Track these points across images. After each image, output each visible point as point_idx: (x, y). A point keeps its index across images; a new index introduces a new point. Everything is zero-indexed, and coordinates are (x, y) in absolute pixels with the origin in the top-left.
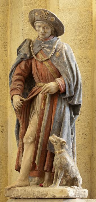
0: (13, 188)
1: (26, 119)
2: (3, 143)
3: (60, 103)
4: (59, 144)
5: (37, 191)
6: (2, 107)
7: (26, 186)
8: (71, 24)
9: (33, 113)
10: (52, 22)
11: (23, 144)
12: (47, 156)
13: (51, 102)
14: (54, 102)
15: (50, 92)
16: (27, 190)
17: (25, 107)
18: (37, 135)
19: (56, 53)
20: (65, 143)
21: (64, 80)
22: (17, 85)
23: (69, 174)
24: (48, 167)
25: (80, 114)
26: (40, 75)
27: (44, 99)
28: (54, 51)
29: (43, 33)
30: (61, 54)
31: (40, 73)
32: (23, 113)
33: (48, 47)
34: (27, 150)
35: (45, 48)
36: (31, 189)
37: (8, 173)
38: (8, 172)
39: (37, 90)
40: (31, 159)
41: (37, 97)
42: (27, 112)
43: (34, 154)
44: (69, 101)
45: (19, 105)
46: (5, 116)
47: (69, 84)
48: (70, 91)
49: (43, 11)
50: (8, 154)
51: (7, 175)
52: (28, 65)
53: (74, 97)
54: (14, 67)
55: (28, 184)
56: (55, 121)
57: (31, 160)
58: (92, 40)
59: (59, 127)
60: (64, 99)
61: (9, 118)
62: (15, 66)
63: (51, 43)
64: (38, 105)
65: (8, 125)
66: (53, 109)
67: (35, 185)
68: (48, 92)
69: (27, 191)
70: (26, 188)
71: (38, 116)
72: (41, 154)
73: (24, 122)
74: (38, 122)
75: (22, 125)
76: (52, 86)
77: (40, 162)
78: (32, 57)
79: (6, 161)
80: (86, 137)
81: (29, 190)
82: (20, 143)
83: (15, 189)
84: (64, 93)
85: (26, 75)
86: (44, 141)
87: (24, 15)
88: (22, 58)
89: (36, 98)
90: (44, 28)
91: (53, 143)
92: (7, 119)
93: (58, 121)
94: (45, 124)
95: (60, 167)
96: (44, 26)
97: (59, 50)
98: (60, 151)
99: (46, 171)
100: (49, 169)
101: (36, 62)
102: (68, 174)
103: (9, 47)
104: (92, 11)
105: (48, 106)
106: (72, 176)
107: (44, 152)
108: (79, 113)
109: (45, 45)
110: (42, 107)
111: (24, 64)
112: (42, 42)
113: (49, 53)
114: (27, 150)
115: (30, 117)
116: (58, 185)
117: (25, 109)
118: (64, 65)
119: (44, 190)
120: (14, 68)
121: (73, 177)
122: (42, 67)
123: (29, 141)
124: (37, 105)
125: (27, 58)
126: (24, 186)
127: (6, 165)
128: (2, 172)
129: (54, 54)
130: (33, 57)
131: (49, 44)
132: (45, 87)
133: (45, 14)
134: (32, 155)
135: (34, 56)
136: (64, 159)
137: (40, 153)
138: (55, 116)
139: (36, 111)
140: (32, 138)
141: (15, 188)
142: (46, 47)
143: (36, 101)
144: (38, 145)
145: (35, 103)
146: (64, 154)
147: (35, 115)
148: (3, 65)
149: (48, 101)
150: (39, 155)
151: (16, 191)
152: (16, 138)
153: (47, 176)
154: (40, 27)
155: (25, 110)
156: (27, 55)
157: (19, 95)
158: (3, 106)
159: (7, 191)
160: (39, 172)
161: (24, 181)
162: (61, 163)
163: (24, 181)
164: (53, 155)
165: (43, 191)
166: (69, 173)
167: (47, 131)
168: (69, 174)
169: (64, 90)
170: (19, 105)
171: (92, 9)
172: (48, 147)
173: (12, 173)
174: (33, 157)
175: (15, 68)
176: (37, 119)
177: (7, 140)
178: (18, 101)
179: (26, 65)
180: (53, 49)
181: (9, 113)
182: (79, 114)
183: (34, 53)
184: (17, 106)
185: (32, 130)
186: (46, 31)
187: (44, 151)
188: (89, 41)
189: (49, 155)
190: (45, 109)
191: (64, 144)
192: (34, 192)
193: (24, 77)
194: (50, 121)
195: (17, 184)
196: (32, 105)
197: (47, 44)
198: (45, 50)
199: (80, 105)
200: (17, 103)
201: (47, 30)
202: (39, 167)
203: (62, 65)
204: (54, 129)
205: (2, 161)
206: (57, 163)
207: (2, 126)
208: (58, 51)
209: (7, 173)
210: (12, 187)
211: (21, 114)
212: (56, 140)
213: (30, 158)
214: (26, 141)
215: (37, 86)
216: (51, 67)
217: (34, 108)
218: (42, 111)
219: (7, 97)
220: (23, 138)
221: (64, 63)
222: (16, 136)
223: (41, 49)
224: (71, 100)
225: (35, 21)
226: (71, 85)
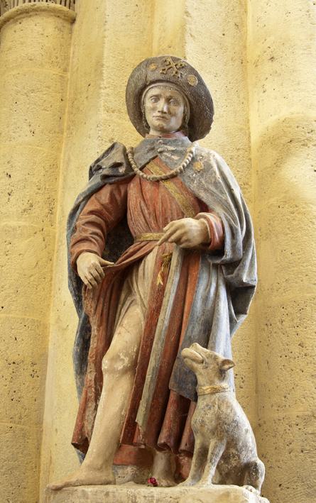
0: (71, 488)
1: (109, 314)
2: (34, 399)
3: (205, 276)
4: (214, 367)
5: (145, 497)
6: (36, 324)
7: (108, 483)
8: (209, 145)
9: (128, 303)
10: (190, 85)
11: (99, 379)
12: (168, 408)
13: (183, 265)
14: (190, 272)
15: (184, 238)
16: (114, 492)
17: (107, 289)
18: (142, 351)
19: (194, 164)
20: (231, 366)
21: (220, 218)
22: (90, 232)
23: (237, 450)
24: (169, 436)
25: (248, 312)
26: (149, 214)
27: (165, 263)
28: (190, 159)
29: (165, 113)
30: (208, 167)
31: (151, 209)
32: (102, 300)
33: (173, 151)
34: (111, 390)
35: (165, 154)
36: (125, 490)
37: (42, 467)
38: (42, 465)
39: (142, 247)
40: (123, 413)
41: (142, 264)
42: (113, 297)
43: (133, 400)
44: (229, 274)
45: (96, 274)
46: (42, 343)
47: (231, 227)
48: (234, 246)
49: (169, 60)
50: (44, 424)
51: (39, 472)
52: (118, 197)
53: (241, 264)
54: (82, 198)
55: (111, 478)
56: (192, 316)
57: (122, 416)
58: (251, 186)
59: (205, 331)
60: (216, 266)
61: (50, 346)
62: (84, 196)
63: (180, 143)
64: (143, 285)
65: (47, 363)
66: (188, 289)
67: (132, 483)
68: (178, 241)
69: (114, 496)
70: (110, 488)
71: (144, 308)
72: (153, 401)
73: (104, 324)
74: (143, 323)
75: (98, 331)
76: (192, 226)
77: (148, 420)
78: (131, 173)
79: (38, 441)
80: (242, 384)
81: (119, 493)
82: (90, 376)
83: (76, 490)
84: (220, 251)
85: (112, 218)
86: (161, 367)
87: (102, 128)
88: (105, 177)
89: (138, 270)
90: (168, 100)
91: (195, 365)
92: (46, 348)
93: (202, 319)
94: (166, 323)
95: (216, 428)
96: (168, 94)
98: (215, 387)
99: (163, 447)
100: (171, 443)
102: (234, 451)
103: (59, 206)
104: (250, 133)
105: (174, 277)
106: (244, 460)
107: (162, 394)
108: (246, 310)
109: (166, 146)
110: (159, 281)
111: (109, 192)
112: (158, 140)
113: (176, 164)
114: (111, 390)
115: (117, 316)
116: (210, 480)
117: (106, 291)
118: (217, 188)
119: (167, 494)
120: (83, 200)
121: (245, 461)
122: (158, 193)
123: (120, 366)
124: (139, 280)
125: (115, 176)
126: (101, 484)
127: (38, 448)
128: (27, 463)
129: (188, 166)
130: (135, 175)
131: (177, 146)
132: (172, 226)
133: (176, 65)
134: (126, 402)
135: (137, 170)
136: (228, 407)
137: (149, 396)
138: (192, 304)
139: (138, 296)
140: (127, 360)
141: (75, 488)
142: (168, 151)
143: (137, 275)
144: (144, 378)
145: (134, 278)
146: (227, 394)
147: (136, 306)
148: (44, 240)
149: (177, 266)
150: (147, 401)
151: (79, 494)
152: (76, 371)
153: (160, 461)
154: (157, 98)
155: (108, 295)
156: (117, 170)
157: (96, 253)
158: (37, 321)
159: (52, 496)
160: (140, 450)
161: (100, 469)
162: (218, 418)
163: (100, 469)
164: (185, 406)
165: (163, 495)
166: (239, 448)
167: (169, 343)
168: (237, 450)
169: (220, 241)
170: (96, 274)
171: (249, 128)
172: (172, 383)
173: (52, 465)
174: (129, 408)
175: (84, 202)
176: (141, 316)
177: (43, 394)
178: (92, 262)
179: (114, 195)
180: (189, 154)
181: (51, 331)
182: (246, 314)
183: (136, 164)
184: (90, 277)
185: (127, 340)
186: (171, 111)
187: (160, 395)
188: (246, 186)
189: (175, 405)
190: (168, 286)
191: (230, 368)
192: (135, 498)
193: (106, 222)
194: (178, 316)
195: (82, 479)
196: (125, 286)
197: (170, 145)
198: (167, 157)
199: (253, 287)
200: (89, 268)
201: (175, 107)
202: (145, 435)
203: (212, 188)
204: (190, 337)
205: (28, 439)
206: (206, 420)
207: (33, 364)
208: (200, 160)
209: (39, 467)
210: (67, 485)
211: (98, 300)
212: (204, 356)
213: (121, 409)
214: (111, 366)
215: (142, 242)
216: (182, 194)
217: (130, 292)
218: (159, 293)
219: (49, 305)
220: (101, 360)
221: (216, 184)
222: (76, 365)
223: (157, 156)
224: (232, 273)
225: (145, 86)
226: (237, 230)
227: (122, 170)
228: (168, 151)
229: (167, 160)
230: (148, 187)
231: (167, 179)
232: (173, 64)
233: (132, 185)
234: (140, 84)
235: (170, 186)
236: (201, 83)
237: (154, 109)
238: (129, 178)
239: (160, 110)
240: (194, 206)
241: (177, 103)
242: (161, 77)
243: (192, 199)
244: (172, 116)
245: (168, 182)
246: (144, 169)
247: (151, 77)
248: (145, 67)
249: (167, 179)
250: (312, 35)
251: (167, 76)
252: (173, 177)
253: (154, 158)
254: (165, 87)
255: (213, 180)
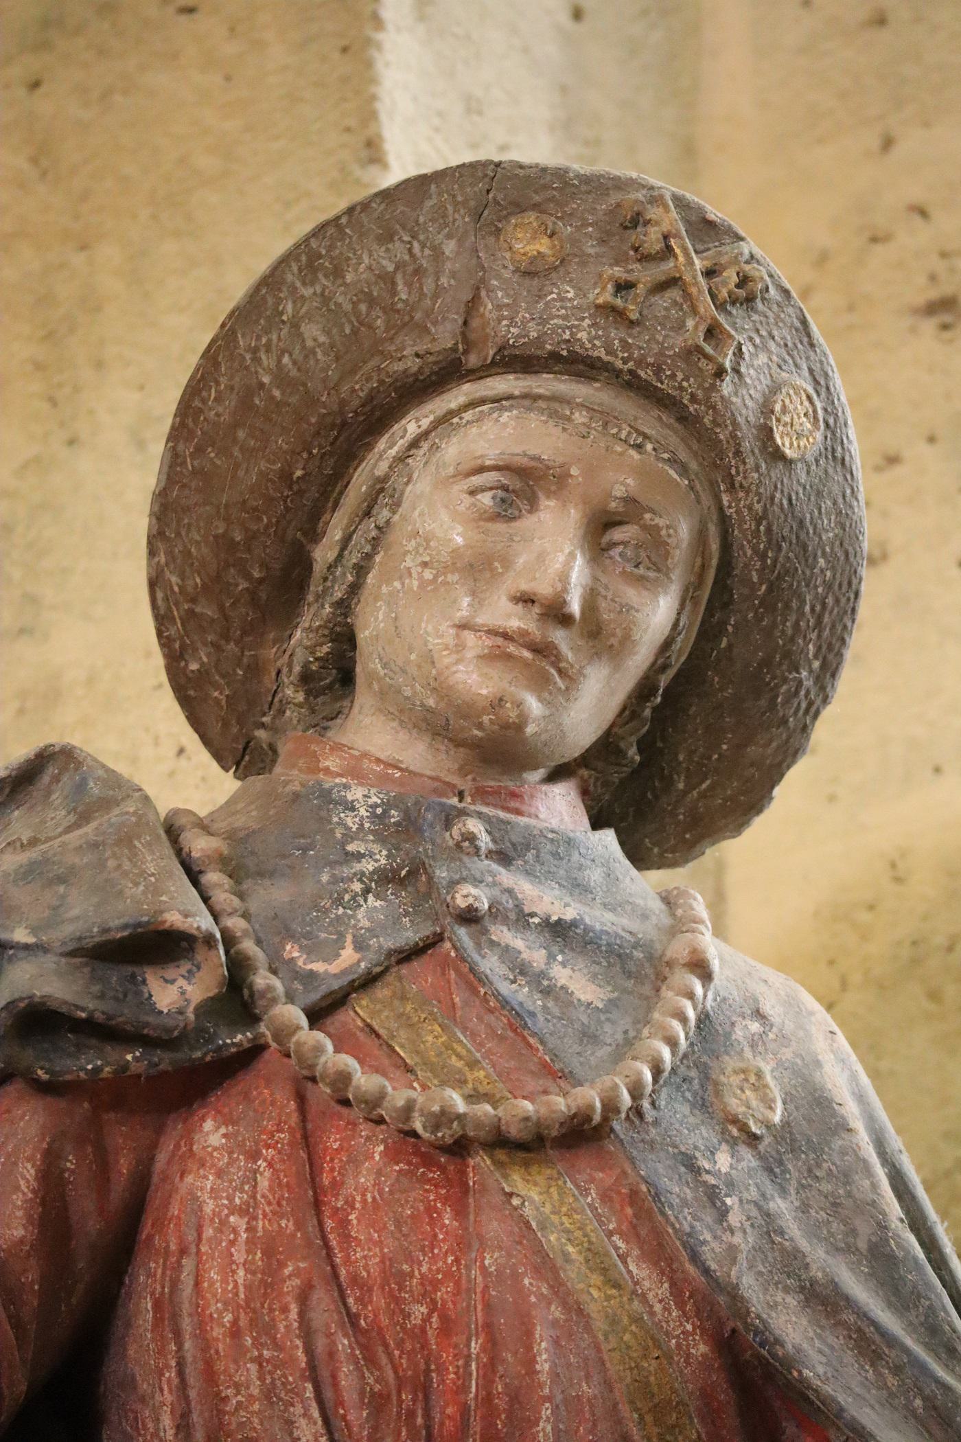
10: (777, 455)
49: (671, 219)
90: (601, 528)
96: (621, 483)
97: (755, 1027)
101: (307, 1140)
109: (506, 877)
131: (440, 804)
133: (709, 273)
154: (521, 486)
198: (521, 969)
225: (448, 372)
227: (175, 993)
228: (521, 919)
229: (520, 994)
230: (366, 1172)
231: (528, 1146)
232: (692, 263)
233: (212, 1134)
234: (407, 357)
235: (538, 1196)
236: (835, 454)
237: (480, 568)
238: (198, 1072)
239: (544, 588)
240: (710, 1411)
241: (651, 559)
242: (586, 336)
243: (701, 1349)
244: (597, 655)
245: (541, 1175)
246: (344, 1017)
247: (510, 318)
248: (463, 219)
249: (528, 1146)
250: (160, 686)
251: (638, 340)
252: (580, 1136)
253: (408, 955)
254: (606, 418)
255: (865, 1230)
